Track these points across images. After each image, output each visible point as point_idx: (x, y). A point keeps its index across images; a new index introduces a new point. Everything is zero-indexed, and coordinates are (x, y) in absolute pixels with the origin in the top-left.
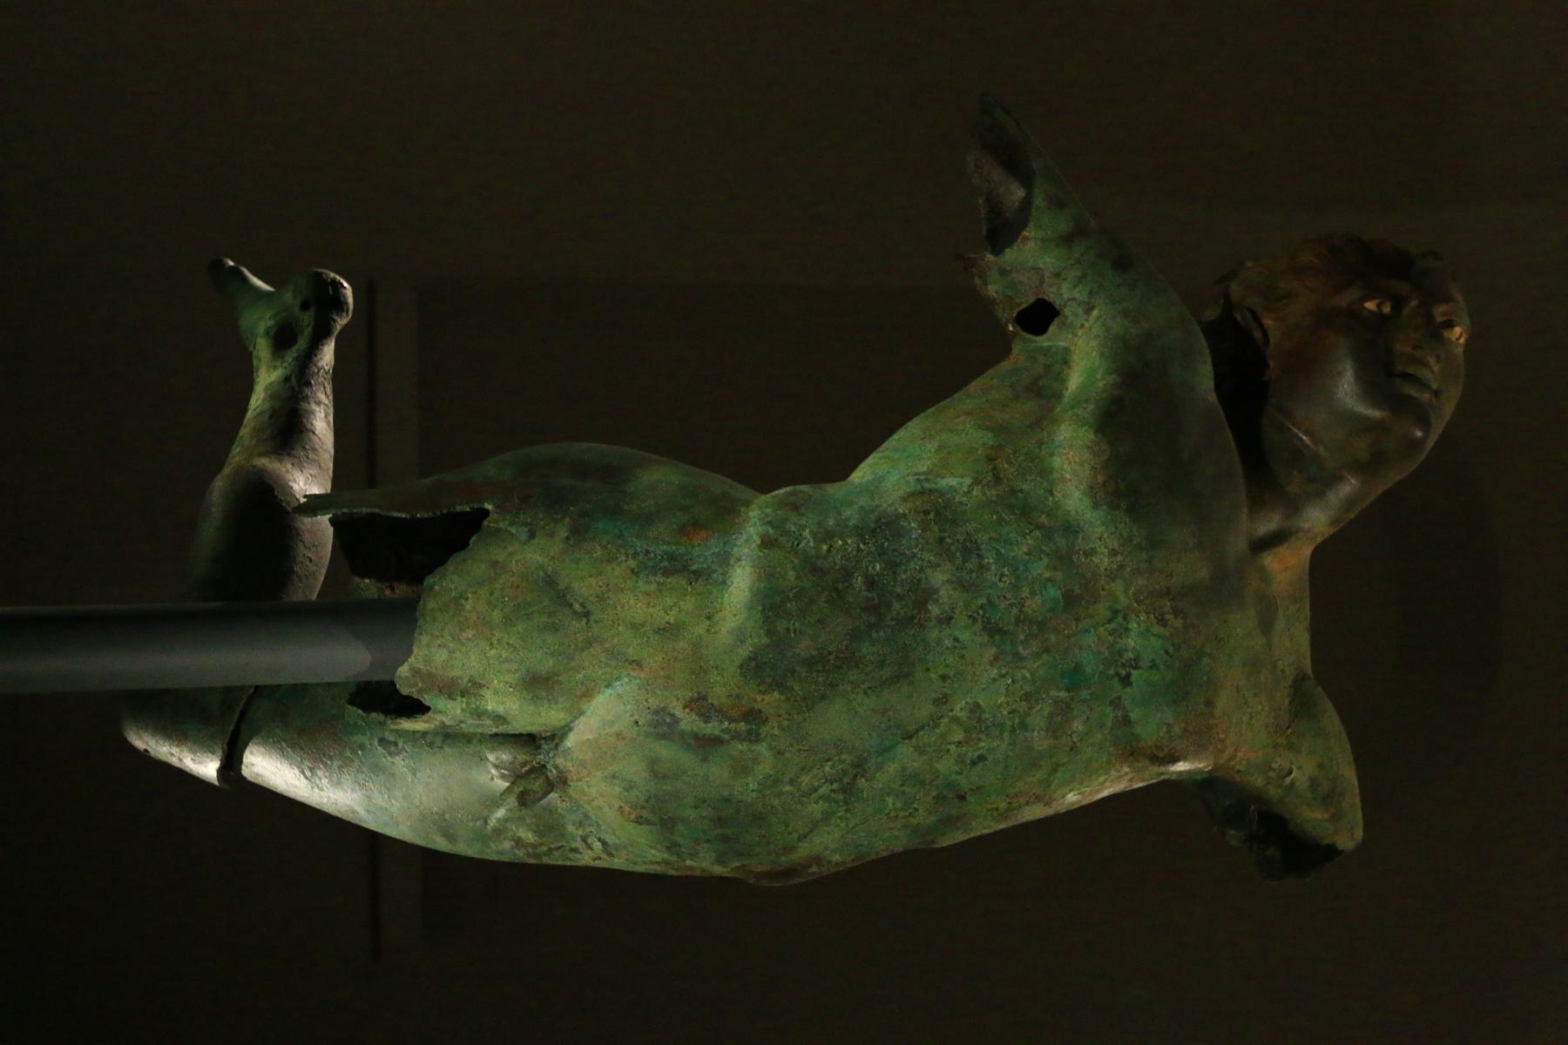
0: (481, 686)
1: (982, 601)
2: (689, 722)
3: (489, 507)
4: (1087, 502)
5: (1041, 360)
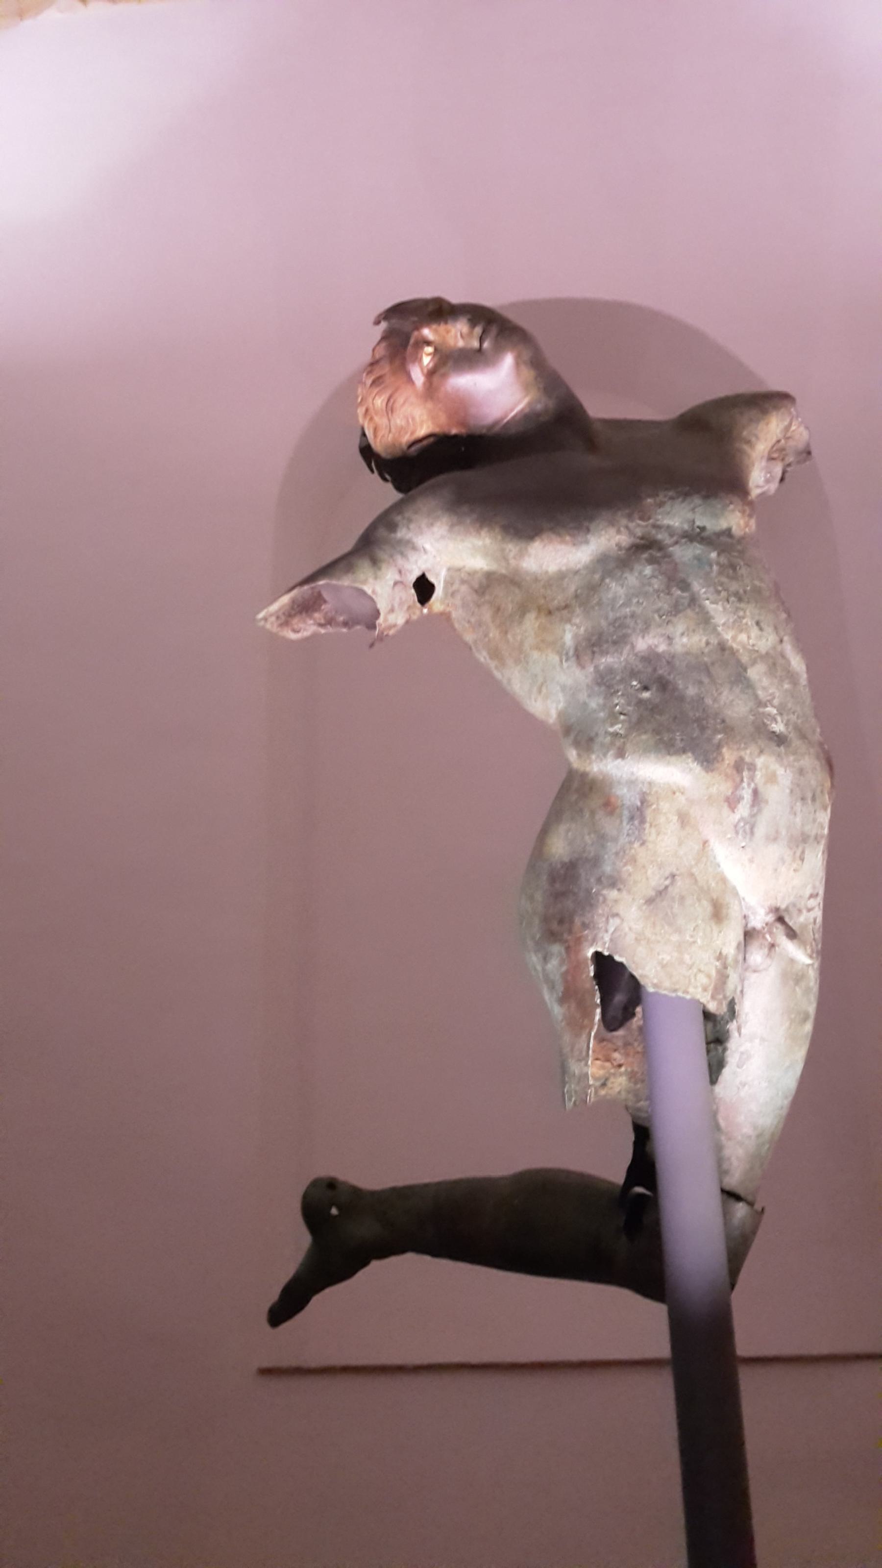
0: (720, 953)
1: (656, 616)
2: (743, 810)
3: (590, 953)
4: (584, 548)
5: (456, 586)
